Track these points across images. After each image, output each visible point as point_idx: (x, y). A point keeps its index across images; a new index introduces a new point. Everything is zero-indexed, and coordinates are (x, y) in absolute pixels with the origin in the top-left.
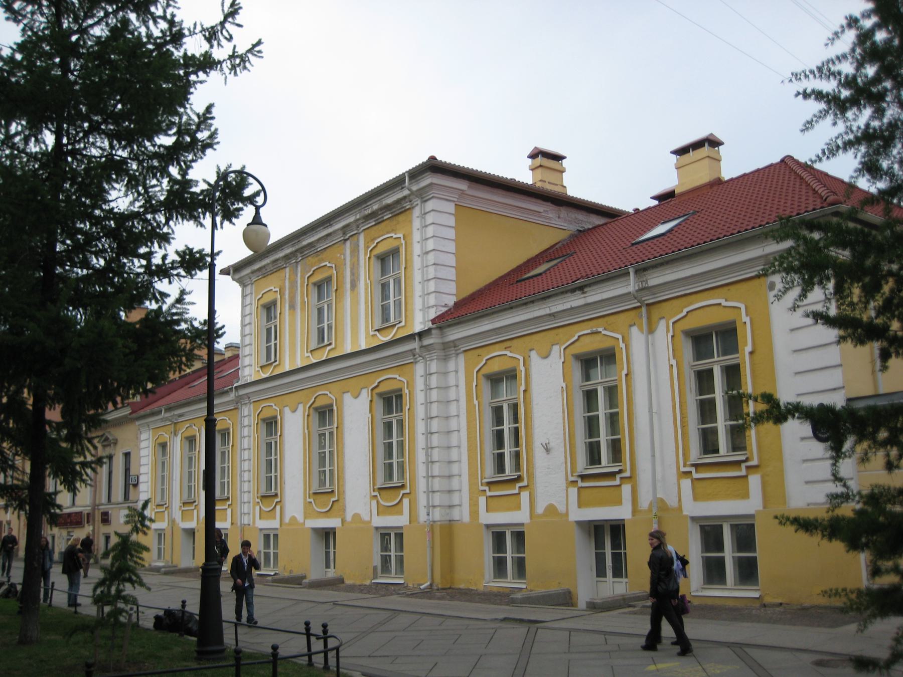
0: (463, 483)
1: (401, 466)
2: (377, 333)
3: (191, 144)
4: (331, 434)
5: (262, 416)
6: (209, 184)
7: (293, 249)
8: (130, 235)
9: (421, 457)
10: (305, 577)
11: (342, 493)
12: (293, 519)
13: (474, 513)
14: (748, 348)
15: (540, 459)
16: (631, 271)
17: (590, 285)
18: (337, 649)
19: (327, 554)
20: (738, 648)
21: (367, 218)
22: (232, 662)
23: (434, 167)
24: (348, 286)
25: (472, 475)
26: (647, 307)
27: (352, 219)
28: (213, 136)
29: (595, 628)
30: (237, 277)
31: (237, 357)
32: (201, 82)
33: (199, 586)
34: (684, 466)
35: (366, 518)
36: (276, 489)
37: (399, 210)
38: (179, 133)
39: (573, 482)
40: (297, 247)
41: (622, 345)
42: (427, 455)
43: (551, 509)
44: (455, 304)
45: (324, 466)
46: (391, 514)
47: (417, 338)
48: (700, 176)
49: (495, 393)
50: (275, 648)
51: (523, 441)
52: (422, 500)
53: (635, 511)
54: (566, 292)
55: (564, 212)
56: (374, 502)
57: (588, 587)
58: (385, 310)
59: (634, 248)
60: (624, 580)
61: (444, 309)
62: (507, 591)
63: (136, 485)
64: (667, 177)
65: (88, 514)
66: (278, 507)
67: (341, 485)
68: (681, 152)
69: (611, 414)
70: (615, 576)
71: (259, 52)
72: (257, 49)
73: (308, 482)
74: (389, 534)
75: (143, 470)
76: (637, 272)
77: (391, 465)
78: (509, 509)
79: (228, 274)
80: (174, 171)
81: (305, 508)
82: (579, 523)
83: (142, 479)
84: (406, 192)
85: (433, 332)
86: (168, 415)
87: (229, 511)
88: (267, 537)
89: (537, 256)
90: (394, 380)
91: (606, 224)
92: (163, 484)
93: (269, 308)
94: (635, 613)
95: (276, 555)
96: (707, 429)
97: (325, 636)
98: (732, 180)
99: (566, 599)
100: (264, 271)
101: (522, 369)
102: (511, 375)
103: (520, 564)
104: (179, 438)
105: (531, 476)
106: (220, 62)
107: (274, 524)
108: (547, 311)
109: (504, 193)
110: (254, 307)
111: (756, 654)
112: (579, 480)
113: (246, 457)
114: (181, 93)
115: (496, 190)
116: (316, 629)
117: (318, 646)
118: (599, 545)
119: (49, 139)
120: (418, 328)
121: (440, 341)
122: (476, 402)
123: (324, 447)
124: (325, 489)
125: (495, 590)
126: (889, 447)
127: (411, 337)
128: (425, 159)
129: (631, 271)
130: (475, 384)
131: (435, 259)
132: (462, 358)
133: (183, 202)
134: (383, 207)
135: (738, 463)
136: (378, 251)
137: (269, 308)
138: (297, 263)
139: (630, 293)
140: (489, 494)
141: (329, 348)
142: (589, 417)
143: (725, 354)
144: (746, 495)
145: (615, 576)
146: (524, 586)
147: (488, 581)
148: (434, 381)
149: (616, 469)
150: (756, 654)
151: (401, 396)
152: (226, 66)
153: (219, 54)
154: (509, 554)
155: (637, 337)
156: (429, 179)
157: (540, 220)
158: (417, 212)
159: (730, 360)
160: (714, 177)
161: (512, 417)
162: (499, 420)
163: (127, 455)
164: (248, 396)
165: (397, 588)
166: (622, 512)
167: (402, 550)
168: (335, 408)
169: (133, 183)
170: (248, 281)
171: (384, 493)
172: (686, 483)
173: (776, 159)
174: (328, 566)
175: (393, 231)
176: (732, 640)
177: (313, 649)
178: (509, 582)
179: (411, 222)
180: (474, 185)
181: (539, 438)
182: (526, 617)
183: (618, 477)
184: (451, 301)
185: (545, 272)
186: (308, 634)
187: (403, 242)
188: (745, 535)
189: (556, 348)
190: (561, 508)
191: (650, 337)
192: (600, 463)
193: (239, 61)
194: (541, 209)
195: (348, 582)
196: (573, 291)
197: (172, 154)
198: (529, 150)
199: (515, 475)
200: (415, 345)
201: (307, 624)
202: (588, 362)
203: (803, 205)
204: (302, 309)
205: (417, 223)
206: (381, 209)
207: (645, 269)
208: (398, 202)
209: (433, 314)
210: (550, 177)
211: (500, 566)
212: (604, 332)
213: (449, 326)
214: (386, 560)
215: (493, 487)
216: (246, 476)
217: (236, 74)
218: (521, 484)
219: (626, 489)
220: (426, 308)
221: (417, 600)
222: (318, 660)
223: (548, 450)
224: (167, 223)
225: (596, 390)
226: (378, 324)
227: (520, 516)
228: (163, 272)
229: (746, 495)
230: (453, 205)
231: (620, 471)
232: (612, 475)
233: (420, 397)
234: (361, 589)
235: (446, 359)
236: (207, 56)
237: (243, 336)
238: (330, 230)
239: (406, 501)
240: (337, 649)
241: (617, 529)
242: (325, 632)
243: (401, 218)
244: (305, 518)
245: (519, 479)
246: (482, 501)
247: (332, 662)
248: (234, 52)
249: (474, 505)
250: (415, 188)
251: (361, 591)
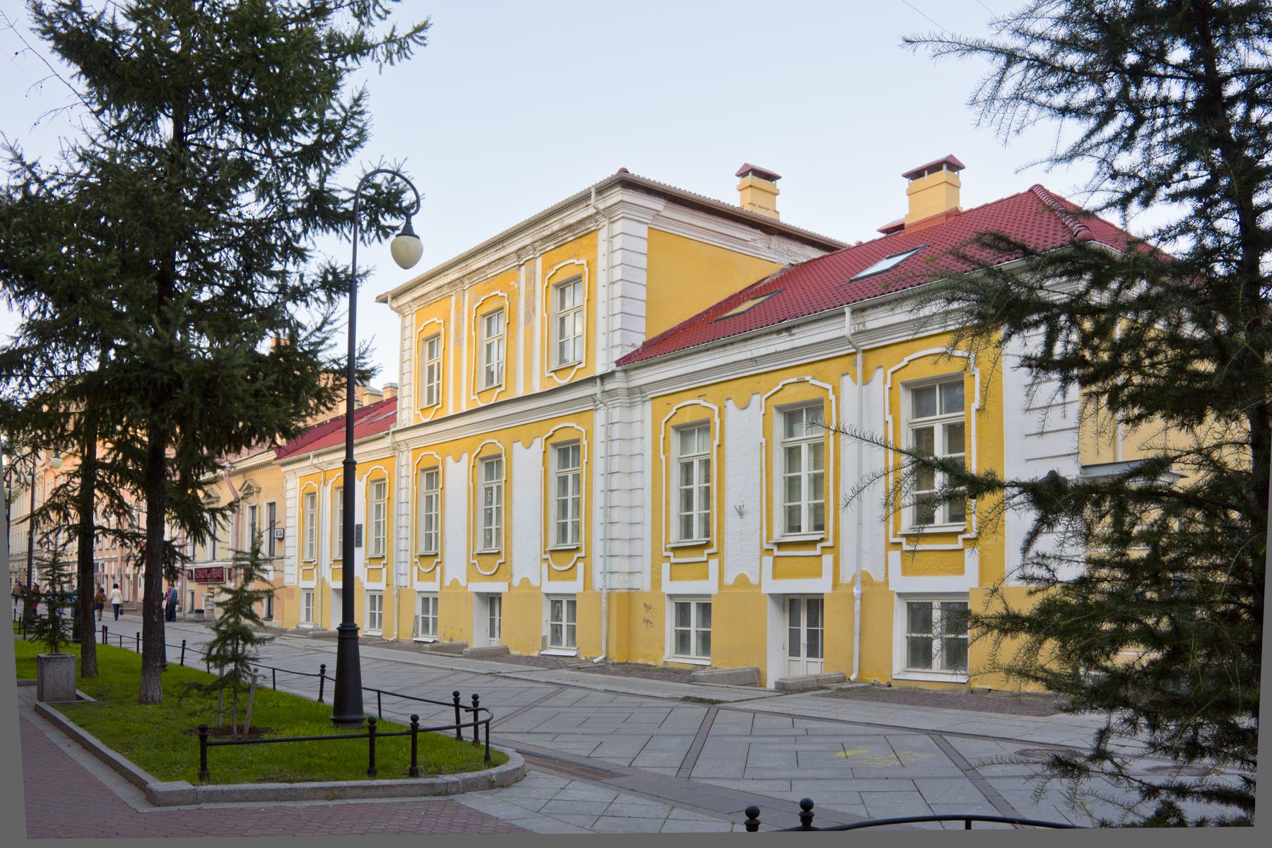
0: (645, 547)
1: (577, 527)
3: (337, 140)
4: (499, 488)
5: (422, 466)
6: (352, 191)
7: (460, 275)
8: (259, 247)
9: (598, 516)
10: (466, 646)
11: (509, 555)
12: (455, 581)
13: (656, 582)
14: (976, 405)
15: (732, 523)
16: (847, 310)
17: (798, 326)
18: (487, 722)
19: (492, 621)
20: (938, 735)
21: (545, 239)
22: (367, 732)
23: (626, 182)
24: (522, 319)
25: (656, 538)
26: (863, 352)
27: (528, 241)
28: (361, 133)
29: (784, 710)
30: (395, 305)
31: (394, 399)
32: (348, 70)
33: (335, 650)
34: (895, 536)
35: (535, 583)
36: (498, 543)
37: (582, 232)
38: (322, 131)
40: (465, 272)
41: (832, 397)
42: (606, 515)
43: (742, 580)
44: (644, 344)
45: (491, 524)
46: (563, 579)
47: (598, 381)
48: (934, 202)
49: (684, 447)
50: (415, 718)
51: (714, 503)
52: (598, 565)
53: (836, 584)
54: (771, 333)
55: (775, 241)
56: (545, 566)
57: (777, 667)
59: (852, 285)
60: (820, 660)
61: (631, 350)
62: (690, 668)
63: (281, 540)
64: (895, 205)
65: (230, 570)
66: (438, 568)
67: (509, 545)
68: (916, 175)
70: (809, 655)
71: (422, 38)
72: (422, 34)
73: (471, 542)
74: (561, 602)
75: (289, 522)
76: (853, 312)
77: (564, 526)
78: (695, 578)
79: (385, 301)
80: (313, 175)
81: (468, 570)
82: (773, 596)
83: (288, 533)
84: (591, 211)
85: (617, 374)
87: (384, 571)
88: (426, 600)
89: (741, 292)
90: (572, 428)
91: (822, 258)
92: (311, 539)
94: (829, 696)
95: (435, 620)
97: (475, 708)
98: (971, 211)
99: (754, 678)
100: (426, 299)
101: (717, 420)
102: (703, 426)
103: (705, 639)
104: (329, 488)
105: (721, 542)
106: (374, 47)
107: (433, 586)
108: (749, 355)
109: (707, 216)
110: (415, 341)
111: (956, 742)
112: (775, 548)
113: (403, 512)
114: (331, 82)
115: (711, 217)
116: (466, 700)
117: (467, 718)
118: (794, 621)
119: (166, 126)
120: (600, 370)
121: (624, 385)
122: (663, 457)
123: (491, 503)
124: (492, 552)
125: (676, 667)
126: (1088, 512)
127: (592, 380)
129: (847, 310)
130: (662, 436)
131: (622, 292)
132: (649, 405)
133: (321, 210)
134: (561, 229)
135: (954, 535)
136: (556, 280)
137: (432, 341)
140: (673, 560)
141: (499, 390)
142: (790, 478)
143: (949, 410)
144: (960, 571)
145: (809, 655)
146: (708, 663)
147: (668, 655)
149: (818, 537)
150: (956, 742)
151: (578, 447)
152: (380, 52)
153: (376, 33)
154: (694, 628)
155: (849, 387)
156: (618, 195)
157: (747, 251)
158: (603, 235)
159: (954, 417)
160: (952, 206)
161: (703, 475)
162: (688, 479)
163: (272, 505)
165: (568, 660)
166: (819, 585)
167: (574, 620)
168: (504, 459)
169: (264, 190)
170: (407, 311)
171: (557, 555)
172: (895, 556)
173: (1024, 189)
174: (492, 635)
175: (575, 256)
176: (933, 727)
177: (462, 722)
178: (693, 658)
179: (595, 247)
180: (671, 205)
181: (733, 498)
182: (706, 697)
183: (819, 546)
184: (639, 340)
185: (748, 310)
186: (457, 705)
187: (586, 269)
189: (756, 398)
190: (754, 580)
191: (865, 388)
193: (397, 46)
194: (748, 237)
195: (513, 652)
196: (779, 332)
197: (310, 155)
198: (738, 167)
199: (703, 540)
200: (596, 389)
201: (456, 694)
202: (791, 415)
203: (1050, 241)
204: (470, 344)
205: (602, 248)
206: (562, 230)
207: (863, 310)
208: (581, 222)
209: (618, 355)
210: (762, 199)
211: (683, 641)
212: (812, 382)
213: (636, 369)
214: (556, 631)
215: (679, 553)
216: (403, 533)
217: (392, 63)
218: (710, 551)
219: (828, 560)
220: (610, 347)
222: (468, 733)
223: (741, 514)
224: (305, 231)
225: (800, 447)
227: (708, 587)
228: (299, 294)
229: (960, 571)
230: (645, 227)
231: (822, 540)
232: (812, 543)
233: (599, 449)
234: (529, 660)
235: (631, 405)
236: (359, 37)
237: (402, 374)
238: (502, 253)
239: (580, 566)
240: (487, 722)
241: (815, 604)
242: (476, 703)
243: (585, 241)
244: (468, 581)
245: (708, 545)
246: (666, 567)
247: (482, 736)
248: (392, 35)
249: (656, 572)
250: (601, 206)
251: (528, 663)
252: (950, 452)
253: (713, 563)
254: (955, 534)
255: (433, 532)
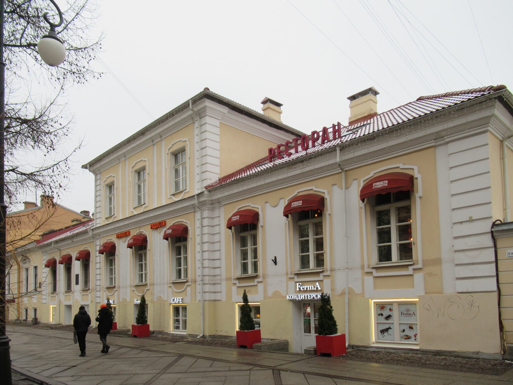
2: (172, 196)
23: (207, 95)
30: (92, 169)
36: (146, 280)
39: (290, 278)
58: (177, 184)
64: (342, 114)
68: (353, 98)
69: (244, 263)
79: (86, 168)
86: (55, 246)
93: (110, 187)
96: (382, 246)
128: (202, 90)
137: (110, 187)
138: (126, 160)
139: (336, 163)
140: (238, 285)
141: (144, 206)
148: (206, 222)
163: (36, 268)
164: (99, 234)
167: (185, 316)
180: (231, 111)
188: (407, 310)
192: (391, 260)
198: (262, 99)
205: (197, 132)
218: (415, 267)
221: (193, 345)
223: (275, 262)
226: (173, 191)
235: (213, 210)
245: (256, 277)
250: (196, 109)
252: (302, 253)
253: (260, 286)
254: (407, 266)
255: (113, 276)
